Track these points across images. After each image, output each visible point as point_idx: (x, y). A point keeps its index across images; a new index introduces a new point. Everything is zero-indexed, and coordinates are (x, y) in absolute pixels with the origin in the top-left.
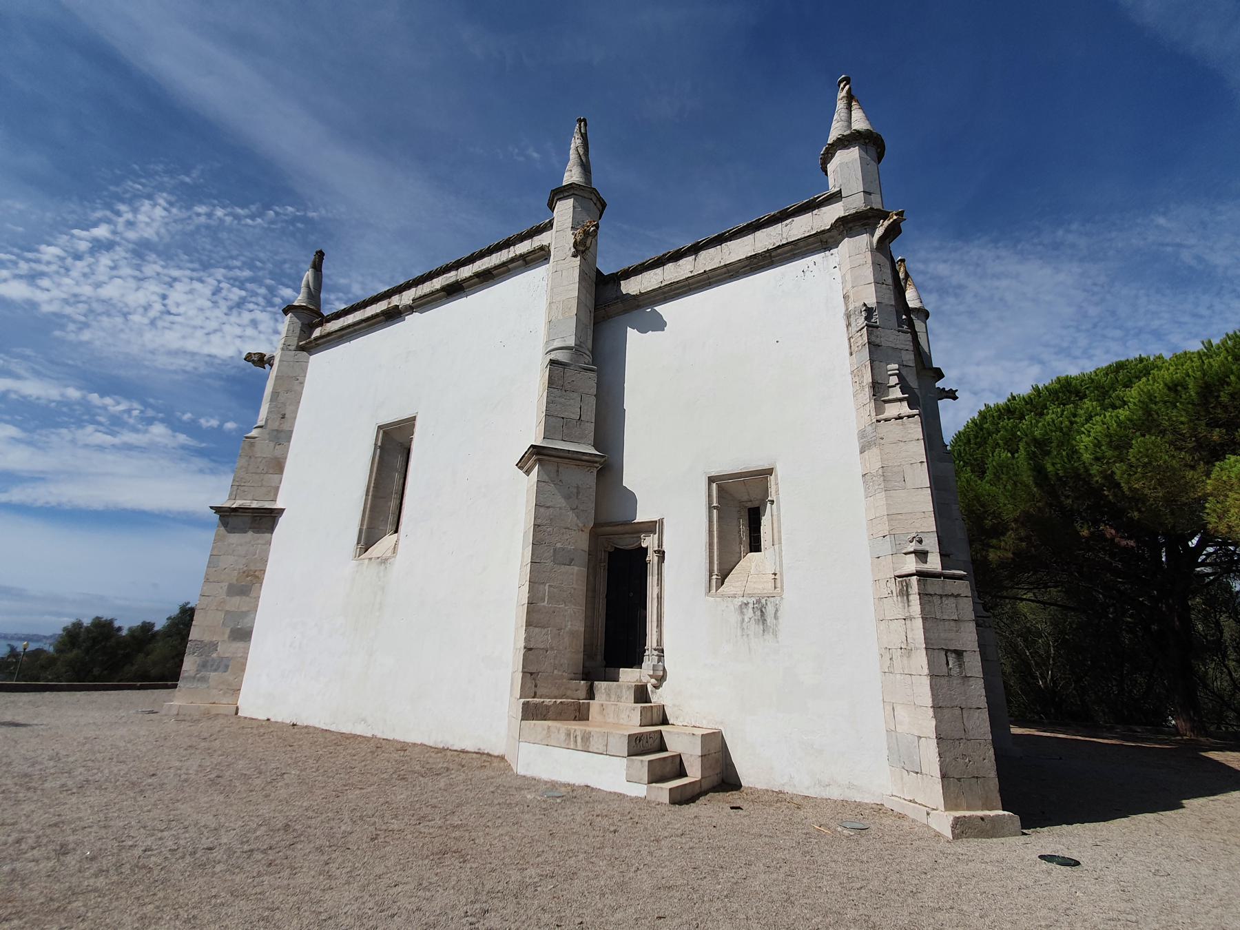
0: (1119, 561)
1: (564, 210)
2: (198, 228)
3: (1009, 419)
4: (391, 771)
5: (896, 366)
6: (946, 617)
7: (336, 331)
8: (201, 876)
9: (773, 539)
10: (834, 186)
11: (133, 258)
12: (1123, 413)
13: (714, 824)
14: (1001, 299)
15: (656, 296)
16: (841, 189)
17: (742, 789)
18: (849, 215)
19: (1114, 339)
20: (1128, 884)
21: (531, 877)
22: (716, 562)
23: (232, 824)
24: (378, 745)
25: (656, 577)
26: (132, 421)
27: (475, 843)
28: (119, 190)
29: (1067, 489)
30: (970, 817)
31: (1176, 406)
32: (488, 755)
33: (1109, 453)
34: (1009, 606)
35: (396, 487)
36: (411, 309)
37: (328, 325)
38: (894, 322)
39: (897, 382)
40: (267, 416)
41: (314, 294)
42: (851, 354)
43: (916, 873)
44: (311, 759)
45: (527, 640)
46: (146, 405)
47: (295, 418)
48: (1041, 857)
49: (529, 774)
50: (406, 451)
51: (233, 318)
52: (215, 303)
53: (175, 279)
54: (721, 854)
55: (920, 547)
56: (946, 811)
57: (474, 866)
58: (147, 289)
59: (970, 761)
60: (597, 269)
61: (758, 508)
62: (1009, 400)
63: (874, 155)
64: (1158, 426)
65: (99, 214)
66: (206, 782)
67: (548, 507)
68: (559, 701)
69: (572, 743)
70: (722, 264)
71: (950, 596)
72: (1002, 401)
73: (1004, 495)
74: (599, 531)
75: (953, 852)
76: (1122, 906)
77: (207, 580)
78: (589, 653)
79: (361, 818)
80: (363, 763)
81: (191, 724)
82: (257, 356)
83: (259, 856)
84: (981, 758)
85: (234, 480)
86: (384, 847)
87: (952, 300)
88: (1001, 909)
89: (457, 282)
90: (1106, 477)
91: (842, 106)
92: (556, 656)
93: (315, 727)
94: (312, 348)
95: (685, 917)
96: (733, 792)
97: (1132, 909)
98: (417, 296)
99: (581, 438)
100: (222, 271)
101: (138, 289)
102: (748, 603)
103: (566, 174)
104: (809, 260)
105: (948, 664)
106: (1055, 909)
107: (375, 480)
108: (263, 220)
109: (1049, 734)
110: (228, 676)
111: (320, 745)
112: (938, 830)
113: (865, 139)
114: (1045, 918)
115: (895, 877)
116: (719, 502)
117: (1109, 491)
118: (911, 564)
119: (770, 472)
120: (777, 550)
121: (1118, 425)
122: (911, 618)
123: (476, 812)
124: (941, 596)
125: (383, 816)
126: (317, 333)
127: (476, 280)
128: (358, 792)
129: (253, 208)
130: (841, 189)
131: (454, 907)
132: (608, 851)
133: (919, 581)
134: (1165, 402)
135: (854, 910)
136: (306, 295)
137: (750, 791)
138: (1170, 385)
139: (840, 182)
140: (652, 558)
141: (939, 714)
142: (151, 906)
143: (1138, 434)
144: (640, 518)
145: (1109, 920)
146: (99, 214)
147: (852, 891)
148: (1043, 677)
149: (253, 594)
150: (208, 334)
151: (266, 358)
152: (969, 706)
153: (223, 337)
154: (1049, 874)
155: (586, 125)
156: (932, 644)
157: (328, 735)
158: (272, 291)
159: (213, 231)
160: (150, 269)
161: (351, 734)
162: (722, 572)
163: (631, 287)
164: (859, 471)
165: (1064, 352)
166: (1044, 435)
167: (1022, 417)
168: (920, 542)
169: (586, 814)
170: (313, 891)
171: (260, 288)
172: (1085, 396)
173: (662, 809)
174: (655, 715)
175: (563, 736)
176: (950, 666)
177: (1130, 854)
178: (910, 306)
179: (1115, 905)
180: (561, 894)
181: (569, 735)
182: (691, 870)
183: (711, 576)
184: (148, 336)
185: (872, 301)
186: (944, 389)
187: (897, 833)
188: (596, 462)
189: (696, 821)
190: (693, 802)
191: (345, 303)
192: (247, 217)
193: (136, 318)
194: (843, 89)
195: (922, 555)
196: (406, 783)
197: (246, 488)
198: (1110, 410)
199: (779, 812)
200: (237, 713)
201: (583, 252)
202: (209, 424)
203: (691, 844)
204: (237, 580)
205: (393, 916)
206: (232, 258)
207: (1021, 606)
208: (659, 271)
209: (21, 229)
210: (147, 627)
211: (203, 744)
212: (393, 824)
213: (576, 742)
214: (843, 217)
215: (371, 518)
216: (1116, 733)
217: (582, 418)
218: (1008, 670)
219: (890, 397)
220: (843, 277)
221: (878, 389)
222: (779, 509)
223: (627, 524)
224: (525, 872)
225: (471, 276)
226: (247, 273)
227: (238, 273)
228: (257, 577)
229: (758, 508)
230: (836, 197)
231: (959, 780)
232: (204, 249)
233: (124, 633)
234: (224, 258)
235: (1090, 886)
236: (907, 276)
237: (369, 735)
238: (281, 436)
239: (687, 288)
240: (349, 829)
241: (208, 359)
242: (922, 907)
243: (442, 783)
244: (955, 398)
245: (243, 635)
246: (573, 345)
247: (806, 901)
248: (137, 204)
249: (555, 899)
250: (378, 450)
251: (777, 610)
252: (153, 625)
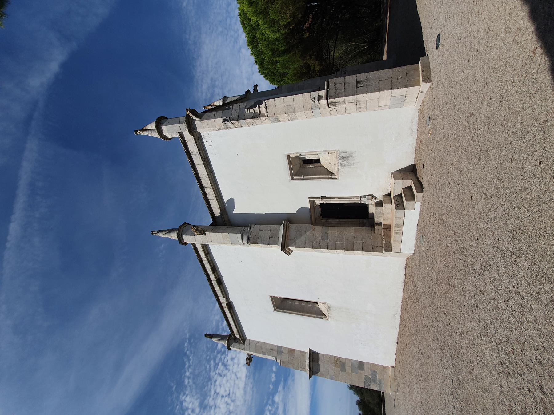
0: (318, 21)
1: (187, 239)
2: (194, 383)
3: (264, 64)
4: (415, 305)
5: (246, 109)
6: (344, 87)
7: (237, 329)
8: (464, 385)
9: (315, 154)
10: (177, 135)
11: (207, 409)
12: (261, 22)
13: (431, 175)
14: (216, 64)
15: (220, 202)
16: (178, 133)
17: (415, 164)
18: (188, 129)
19: (231, 21)
20: (447, 15)
21: (457, 250)
22: (325, 176)
23: (442, 372)
24: (404, 309)
25: (332, 200)
26: (274, 410)
27: (444, 272)
29: (291, 42)
30: (422, 76)
31: (258, 3)
32: (406, 264)
33: (276, 26)
34: (336, 61)
35: (299, 303)
36: (227, 299)
37: (234, 332)
38: (229, 111)
39: (252, 109)
40: (272, 356)
41: (222, 338)
42: (242, 127)
43: (446, 97)
44: (412, 338)
46: (267, 404)
47: (272, 345)
48: (437, 49)
49: (413, 249)
50: (284, 300)
51: (231, 368)
52: (224, 376)
53: (215, 392)
54: (443, 173)
55: (317, 98)
56: (420, 85)
57: (454, 273)
58: (219, 404)
60: (210, 225)
61: (303, 160)
62: (257, 64)
63: (165, 120)
64: (265, 9)
66: (424, 382)
68: (383, 237)
69: (400, 232)
70: (208, 177)
71: (335, 86)
72: (257, 67)
73: (294, 65)
74: (314, 222)
75: (437, 82)
76: (456, 18)
77: (339, 380)
78: (363, 225)
79: (436, 318)
80: (413, 316)
81: (399, 386)
82: (248, 361)
83: (455, 361)
84: (399, 72)
85: (298, 369)
86: (448, 309)
87: (217, 83)
88: (460, 64)
89: (217, 281)
90: (286, 28)
91: (146, 133)
92: (365, 238)
93: (398, 335)
94: (244, 338)
95: (471, 188)
96: (417, 167)
97: (457, 14)
98: (222, 296)
99: (277, 230)
100: (211, 373)
101: (220, 408)
102: (341, 163)
103: (173, 238)
104: (206, 144)
106: (458, 44)
107: (296, 312)
108: (190, 356)
109: (386, 44)
110: (378, 371)
111: (406, 333)
112: (428, 88)
114: (462, 48)
115: (449, 105)
116: (301, 176)
117: (291, 26)
118: (323, 102)
119: (289, 156)
120: (319, 153)
121: (265, 24)
122: (345, 101)
123: (431, 271)
124: (335, 90)
125: (435, 309)
126: (238, 336)
127: (215, 273)
128: (425, 318)
129: (185, 360)
130: (178, 133)
131: (472, 282)
132: (444, 218)
133: (330, 99)
134: (256, 7)
135: (464, 122)
136: (223, 341)
137: (416, 161)
138: (250, 5)
139: (175, 133)
140: (324, 201)
141: (382, 89)
142: (478, 407)
143: (269, 16)
144: (308, 206)
145: (462, 23)
147: (456, 122)
148: (364, 47)
149: (344, 361)
150: (237, 378)
151: (248, 357)
152: (378, 78)
153: (238, 372)
154: (444, 46)
155: (154, 231)
156: (355, 93)
157: (401, 330)
158: (219, 352)
159: (195, 377)
160: (211, 403)
161: (400, 320)
162: (329, 174)
163: (217, 212)
164: (288, 122)
165: (236, 40)
166: (270, 51)
167: (264, 59)
168: (314, 98)
169: (429, 226)
170: (468, 340)
171: (218, 357)
172: (255, 36)
173: (426, 196)
174: (387, 199)
175: (398, 235)
177: (434, 14)
178: (222, 104)
179: (455, 21)
180: (464, 238)
181: (397, 233)
182: (451, 185)
183: (330, 178)
184: (238, 403)
185: (221, 120)
186: (253, 90)
187: (430, 104)
188: (287, 224)
189: (430, 182)
190: (422, 183)
191: (223, 322)
192: (189, 362)
193: (231, 408)
194: (139, 133)
195: (320, 98)
196: (420, 299)
197: (301, 365)
198: (260, 26)
199: (424, 149)
200: (394, 367)
201: (204, 231)
202: (274, 377)
203: (440, 185)
204: (339, 368)
205: (478, 307)
206: (206, 368)
207: (336, 55)
208: (211, 201)
210: (359, 403)
211: (407, 382)
212: (438, 305)
213: (399, 230)
214: (189, 132)
215: (312, 313)
216: (384, 18)
217: (270, 230)
218: (361, 60)
219: (258, 111)
220: (212, 131)
221: (255, 116)
222: (303, 153)
223: (311, 211)
224: (455, 252)
225: (214, 275)
226: (212, 362)
227: (212, 366)
228: (337, 359)
229: (303, 160)
230: (181, 134)
231: (408, 81)
232: (202, 380)
233: (361, 412)
234: (206, 372)
235: (448, 30)
236: (210, 105)
237: (400, 312)
238: (279, 350)
239: (217, 190)
240: (441, 323)
241: (247, 378)
242: (460, 95)
243: (419, 284)
244: (257, 85)
245: (361, 365)
246: (241, 234)
247: (461, 140)
248: (184, 408)
249: (466, 240)
250: (284, 311)
251: (343, 152)
252: (358, 401)
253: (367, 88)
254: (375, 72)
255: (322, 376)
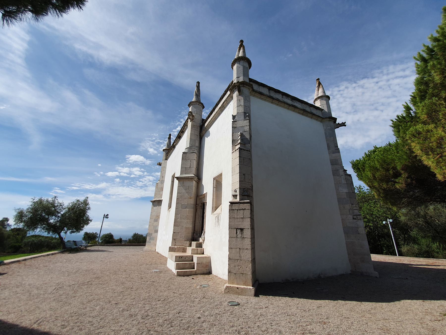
28: (180, 115)
45: (174, 230)
59: (240, 268)
65: (177, 124)
67: (180, 193)
71: (241, 210)
105: (237, 233)
113: (238, 60)
124: (238, 210)
146: (177, 124)
176: (238, 234)
200: (155, 251)
209: (163, 133)
217: (191, 167)
231: (235, 274)
244: (345, 126)
245: (156, 231)
253: (234, 237)
254: (250, 246)
255: (152, 208)
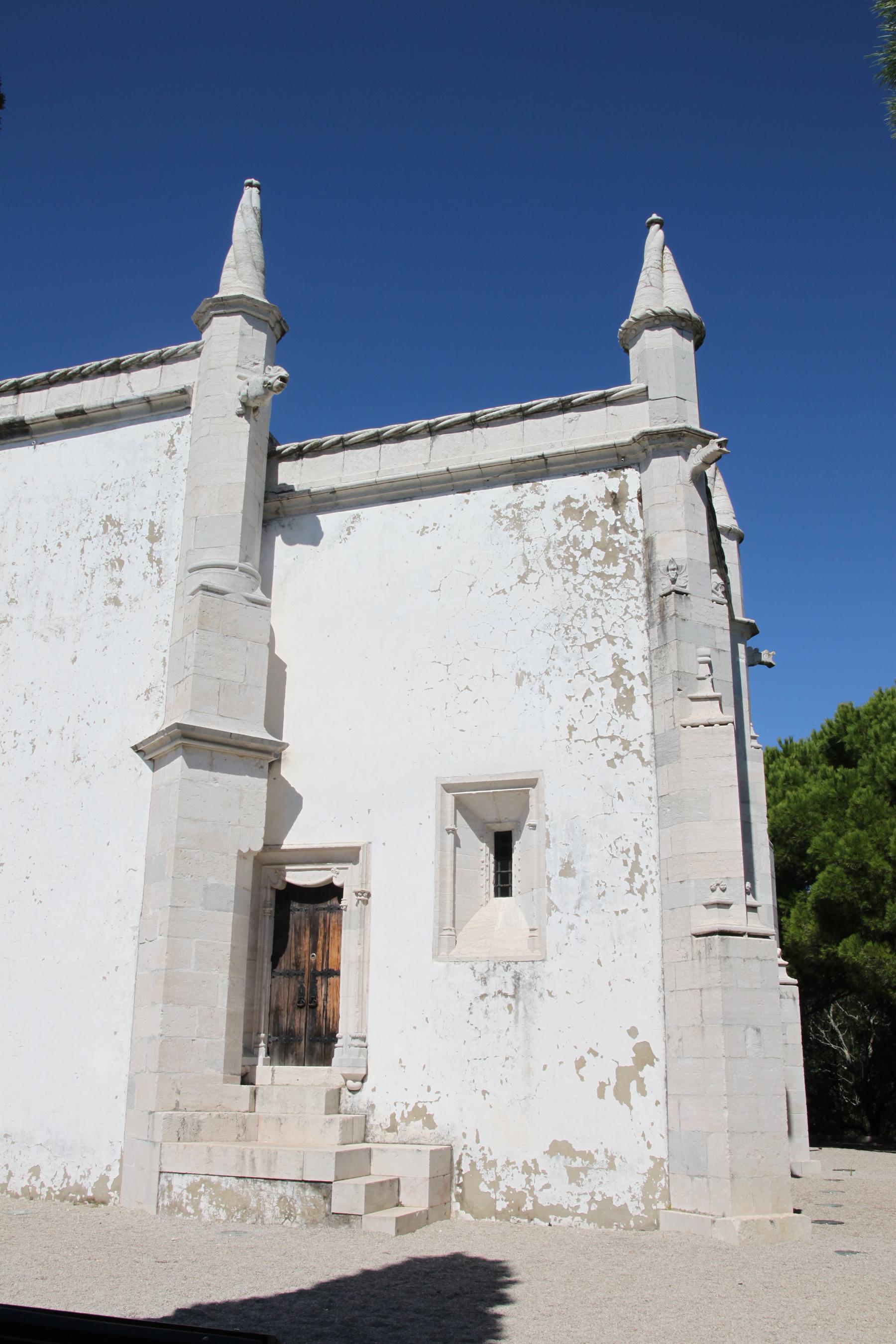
16: (647, 388)
119: (533, 783)
130: (647, 388)
